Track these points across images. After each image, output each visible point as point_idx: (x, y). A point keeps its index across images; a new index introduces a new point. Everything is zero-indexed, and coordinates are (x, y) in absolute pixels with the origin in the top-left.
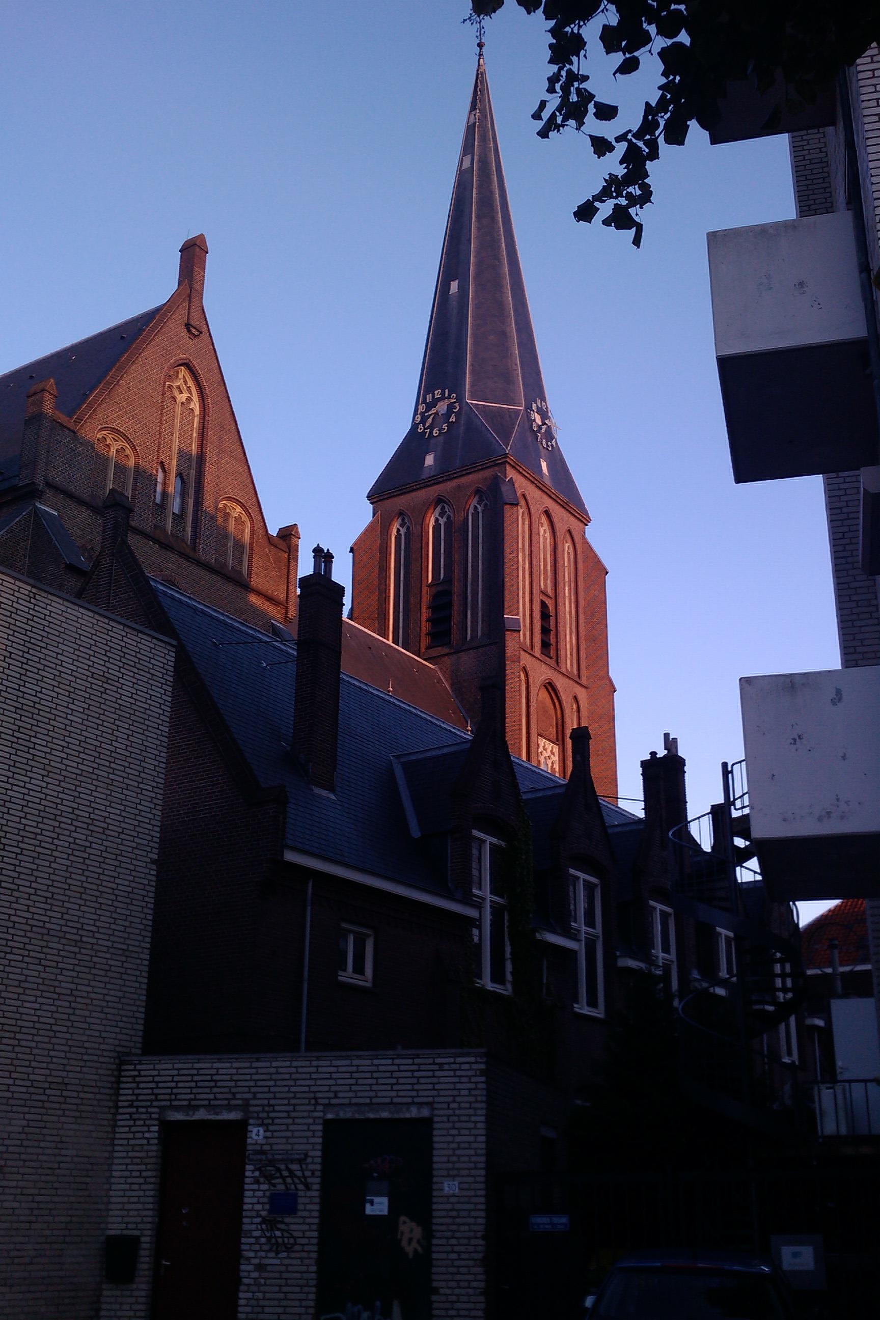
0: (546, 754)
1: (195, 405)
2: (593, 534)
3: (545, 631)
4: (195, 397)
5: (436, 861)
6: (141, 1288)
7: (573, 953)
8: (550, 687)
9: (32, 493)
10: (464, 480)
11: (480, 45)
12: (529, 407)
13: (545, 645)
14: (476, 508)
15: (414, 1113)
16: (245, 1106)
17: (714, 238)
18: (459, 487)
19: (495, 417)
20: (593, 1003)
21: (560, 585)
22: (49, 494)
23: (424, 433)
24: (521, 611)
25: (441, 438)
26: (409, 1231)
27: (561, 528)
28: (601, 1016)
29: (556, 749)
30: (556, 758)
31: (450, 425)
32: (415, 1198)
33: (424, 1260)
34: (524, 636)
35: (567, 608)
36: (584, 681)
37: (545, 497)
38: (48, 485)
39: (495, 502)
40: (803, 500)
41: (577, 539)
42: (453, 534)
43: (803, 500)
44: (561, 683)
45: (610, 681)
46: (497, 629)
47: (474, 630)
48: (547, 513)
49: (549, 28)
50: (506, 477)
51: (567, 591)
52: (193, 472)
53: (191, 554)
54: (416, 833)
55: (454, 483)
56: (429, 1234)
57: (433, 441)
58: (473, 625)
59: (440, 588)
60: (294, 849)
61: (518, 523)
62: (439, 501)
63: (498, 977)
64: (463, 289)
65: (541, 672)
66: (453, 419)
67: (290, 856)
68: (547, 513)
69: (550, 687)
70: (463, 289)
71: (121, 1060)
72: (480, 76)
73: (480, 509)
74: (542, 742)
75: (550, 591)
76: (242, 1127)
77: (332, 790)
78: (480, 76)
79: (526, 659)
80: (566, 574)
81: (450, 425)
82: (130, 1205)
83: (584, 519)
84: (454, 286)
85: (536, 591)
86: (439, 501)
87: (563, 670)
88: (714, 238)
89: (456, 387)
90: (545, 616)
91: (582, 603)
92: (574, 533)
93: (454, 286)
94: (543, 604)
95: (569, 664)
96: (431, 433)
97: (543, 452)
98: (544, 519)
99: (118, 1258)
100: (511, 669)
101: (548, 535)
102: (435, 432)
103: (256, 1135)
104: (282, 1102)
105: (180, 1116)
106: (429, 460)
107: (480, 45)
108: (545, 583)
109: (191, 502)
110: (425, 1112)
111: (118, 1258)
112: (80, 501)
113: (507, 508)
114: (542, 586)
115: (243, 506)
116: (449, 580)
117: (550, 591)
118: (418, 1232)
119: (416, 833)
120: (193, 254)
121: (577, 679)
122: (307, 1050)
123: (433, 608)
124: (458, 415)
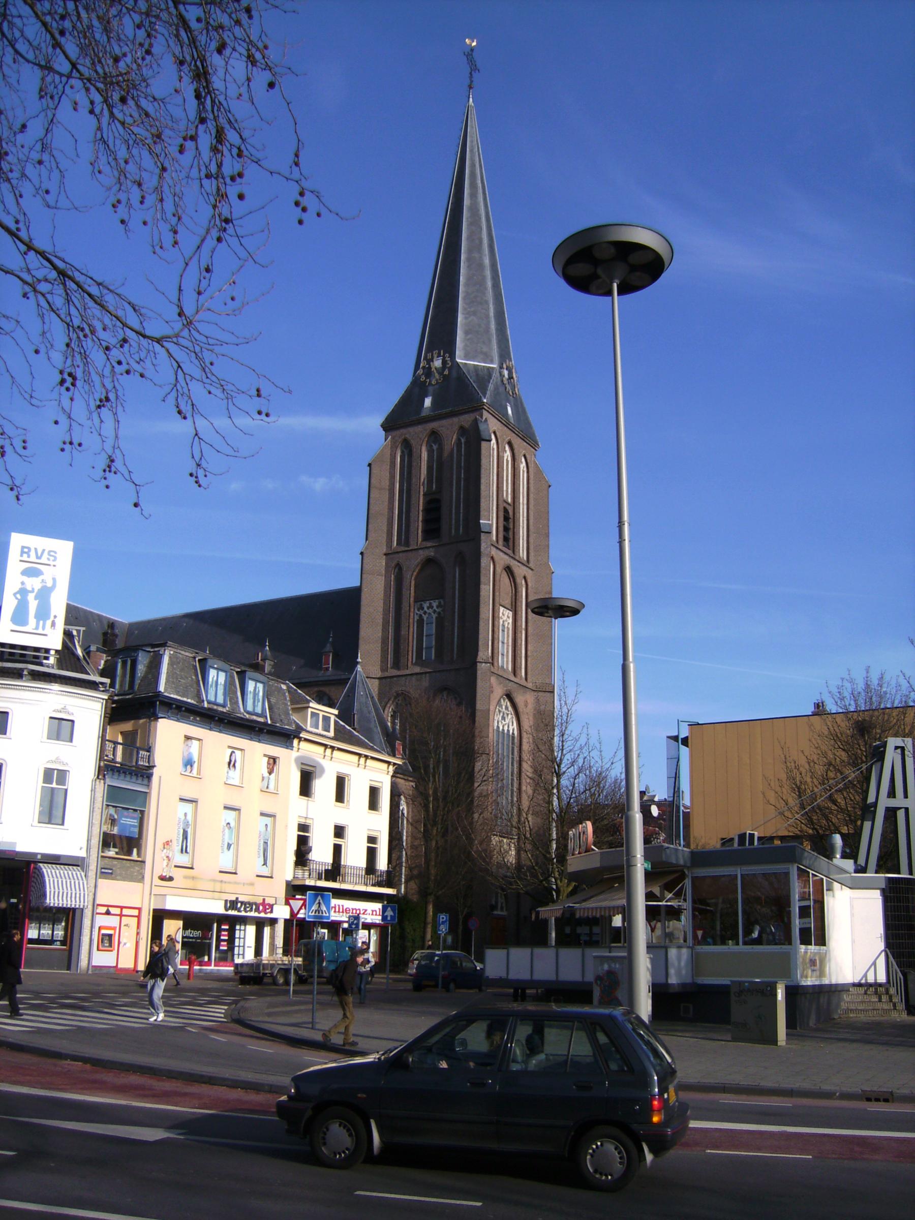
3: (506, 529)
8: (509, 570)
12: (501, 367)
13: (506, 539)
23: (425, 382)
24: (490, 520)
30: (510, 621)
36: (531, 565)
39: (473, 440)
40: (718, 846)
43: (718, 846)
47: (457, 529)
50: (482, 417)
51: (522, 499)
65: (502, 559)
66: (446, 372)
69: (509, 570)
73: (463, 440)
74: (502, 609)
79: (494, 552)
85: (500, 502)
87: (517, 558)
90: (506, 519)
95: (523, 554)
100: (484, 561)
106: (428, 402)
122: (307, 832)
123: (427, 510)
124: (450, 369)
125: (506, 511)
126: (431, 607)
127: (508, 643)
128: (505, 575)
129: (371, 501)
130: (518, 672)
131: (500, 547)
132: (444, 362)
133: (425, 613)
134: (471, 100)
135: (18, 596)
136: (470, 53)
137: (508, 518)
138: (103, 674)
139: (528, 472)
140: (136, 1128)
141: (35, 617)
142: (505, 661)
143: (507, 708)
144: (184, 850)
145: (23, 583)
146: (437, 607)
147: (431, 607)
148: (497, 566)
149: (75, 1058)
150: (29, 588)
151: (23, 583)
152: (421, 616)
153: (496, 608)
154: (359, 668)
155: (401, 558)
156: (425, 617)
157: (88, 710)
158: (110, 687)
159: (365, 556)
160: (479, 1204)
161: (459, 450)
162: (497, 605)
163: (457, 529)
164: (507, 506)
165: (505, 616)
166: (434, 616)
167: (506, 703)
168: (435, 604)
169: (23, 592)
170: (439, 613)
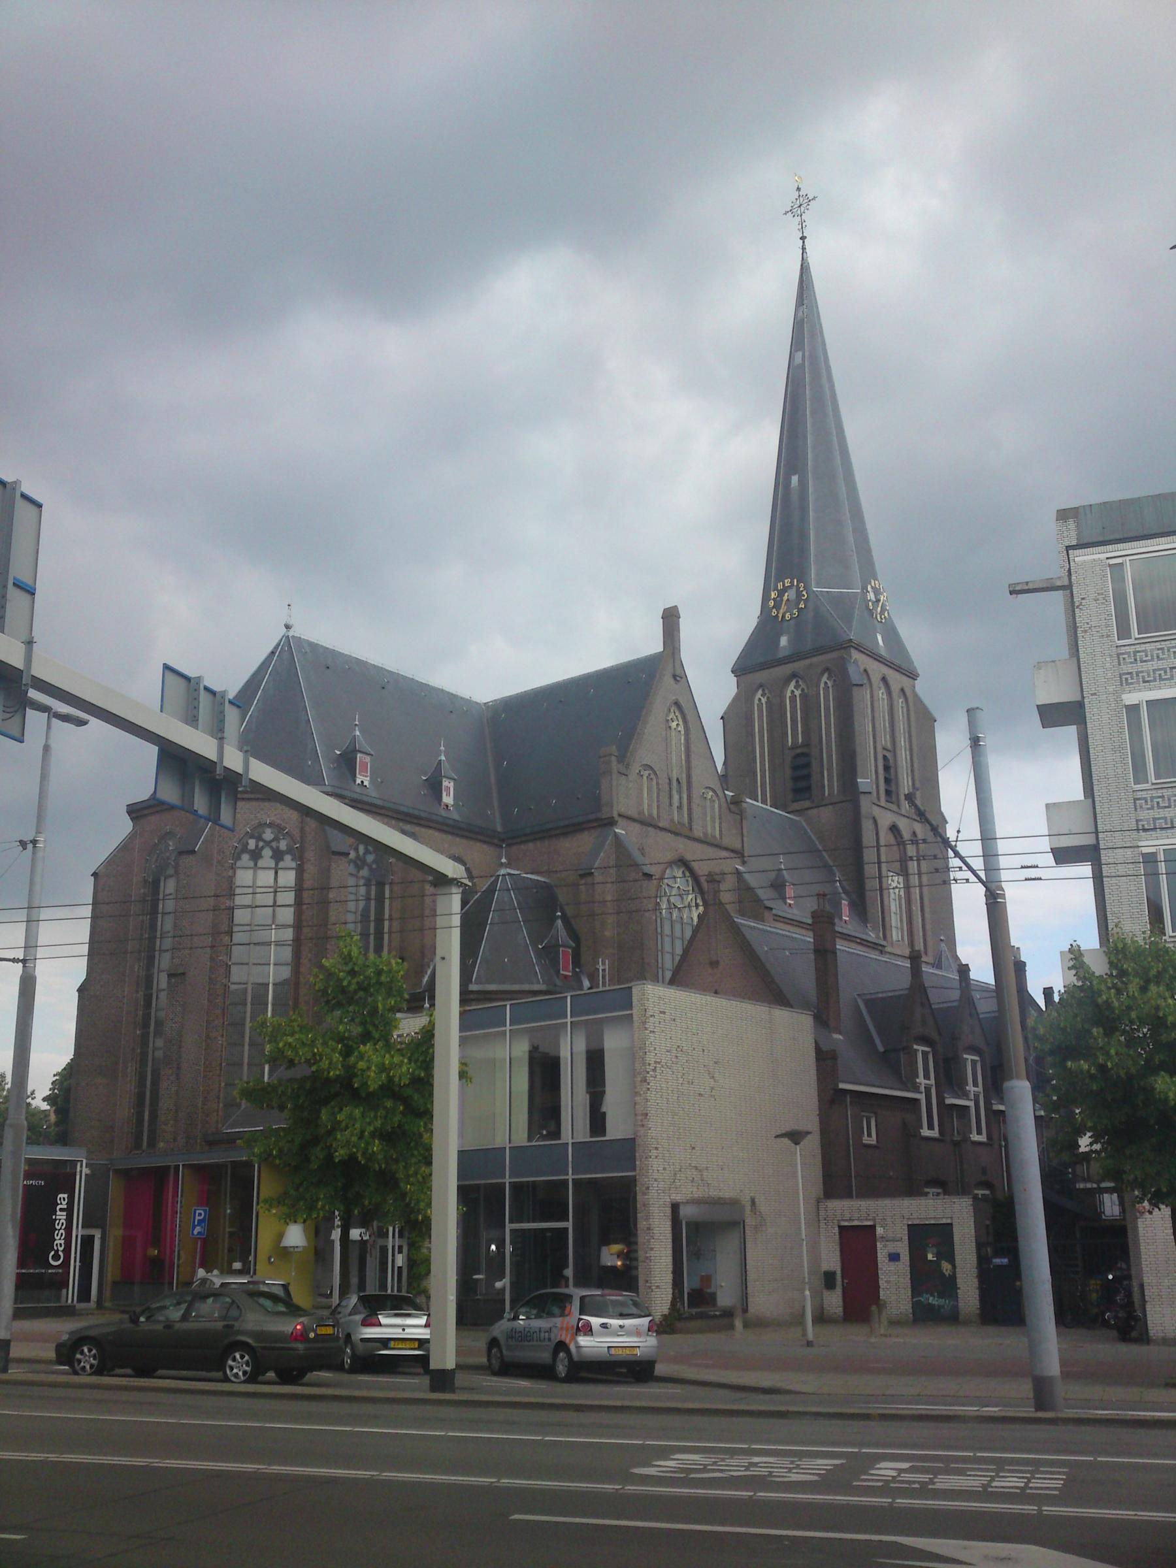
1: (681, 728)
2: (920, 686)
3: (887, 781)
4: (681, 722)
5: (893, 1062)
6: (839, 1290)
7: (967, 1107)
9: (611, 822)
10: (815, 660)
11: (803, 238)
12: (864, 588)
15: (944, 1221)
16: (874, 1220)
17: (1048, 806)
18: (811, 664)
19: (840, 601)
20: (979, 1132)
21: (897, 734)
22: (621, 821)
25: (792, 622)
26: (946, 1267)
27: (895, 688)
28: (985, 1140)
29: (901, 879)
31: (800, 610)
32: (948, 1253)
33: (953, 1277)
35: (903, 756)
37: (882, 666)
38: (620, 815)
41: (909, 693)
42: (809, 704)
44: (903, 824)
45: (942, 814)
46: (850, 791)
48: (884, 679)
51: (902, 742)
52: (684, 776)
53: (689, 834)
54: (881, 1049)
55: (807, 662)
56: (954, 1267)
57: (786, 624)
58: (829, 781)
59: (799, 751)
60: (843, 1082)
61: (862, 699)
62: (794, 676)
63: (931, 1127)
64: (803, 483)
65: (886, 819)
67: (842, 1086)
69: (894, 829)
70: (803, 483)
71: (818, 1201)
72: (804, 269)
73: (830, 684)
75: (889, 746)
76: (873, 1227)
77: (840, 1033)
78: (804, 269)
79: (876, 811)
80: (901, 726)
81: (800, 610)
82: (831, 1260)
83: (913, 676)
84: (795, 479)
86: (794, 676)
88: (1048, 806)
89: (802, 577)
90: (887, 768)
91: (915, 749)
93: (795, 479)
94: (885, 757)
96: (783, 616)
97: (879, 626)
98: (882, 685)
99: (829, 1280)
101: (885, 696)
102: (788, 616)
103: (880, 1231)
104: (892, 1218)
105: (846, 1224)
106: (784, 641)
107: (803, 238)
108: (885, 740)
109: (685, 796)
110: (949, 1221)
111: (829, 1280)
112: (634, 820)
113: (855, 689)
115: (714, 791)
116: (806, 744)
117: (889, 746)
118: (950, 1267)
119: (881, 1049)
120: (671, 618)
121: (891, 675)
124: (806, 601)
164: (888, 754)
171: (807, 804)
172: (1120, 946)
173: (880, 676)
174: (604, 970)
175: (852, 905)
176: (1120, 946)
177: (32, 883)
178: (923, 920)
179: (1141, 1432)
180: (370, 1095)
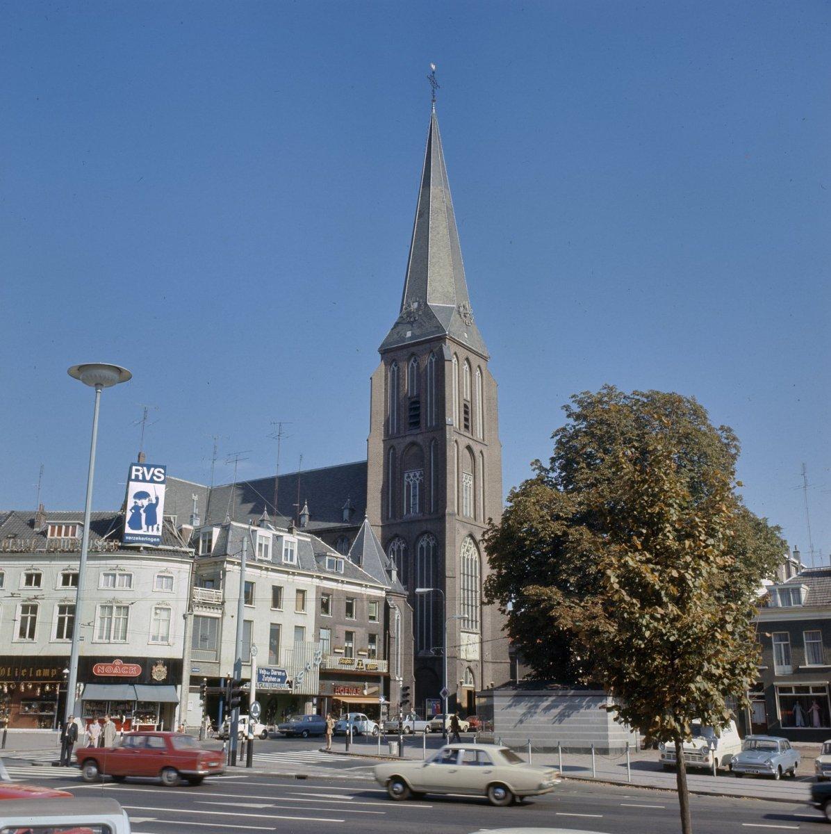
0: (467, 481)
3: (466, 420)
8: (469, 448)
13: (466, 427)
14: (431, 360)
24: (453, 417)
26: (272, 641)
27: (474, 366)
30: (471, 483)
34: (456, 424)
39: (440, 362)
47: (431, 422)
48: (467, 359)
49: (249, 510)
58: (428, 418)
59: (413, 400)
68: (467, 359)
69: (469, 448)
75: (469, 399)
84: (66, 757)
85: (461, 399)
90: (466, 413)
92: (484, 453)
95: (479, 435)
114: (464, 514)
116: (418, 396)
117: (469, 399)
121: (472, 357)
125: (466, 406)
126: (415, 476)
127: (470, 498)
128: (466, 451)
129: (373, 404)
130: (478, 518)
131: (462, 433)
132: (419, 305)
133: (411, 480)
134: (434, 111)
135: (133, 511)
136: (432, 77)
137: (467, 411)
138: (190, 546)
139: (482, 377)
140: (369, 483)
141: (146, 524)
142: (468, 511)
143: (470, 543)
144: (248, 623)
145: (135, 502)
146: (419, 476)
147: (415, 476)
148: (460, 446)
149: (725, 795)
150: (140, 505)
151: (135, 502)
152: (408, 482)
153: (460, 475)
154: (366, 521)
155: (394, 442)
156: (411, 483)
157: (182, 571)
158: (195, 554)
159: (369, 441)
160: (342, 821)
161: (431, 367)
162: (460, 473)
163: (431, 422)
164: (467, 404)
165: (468, 481)
166: (417, 482)
167: (469, 540)
168: (418, 474)
169: (136, 508)
170: (421, 480)
171: (418, 431)
172: (576, 409)
173: (465, 357)
174: (398, 620)
175: (548, 706)
176: (576, 409)
177: (482, 654)
178: (459, 416)
179: (774, 797)
180: (750, 589)
